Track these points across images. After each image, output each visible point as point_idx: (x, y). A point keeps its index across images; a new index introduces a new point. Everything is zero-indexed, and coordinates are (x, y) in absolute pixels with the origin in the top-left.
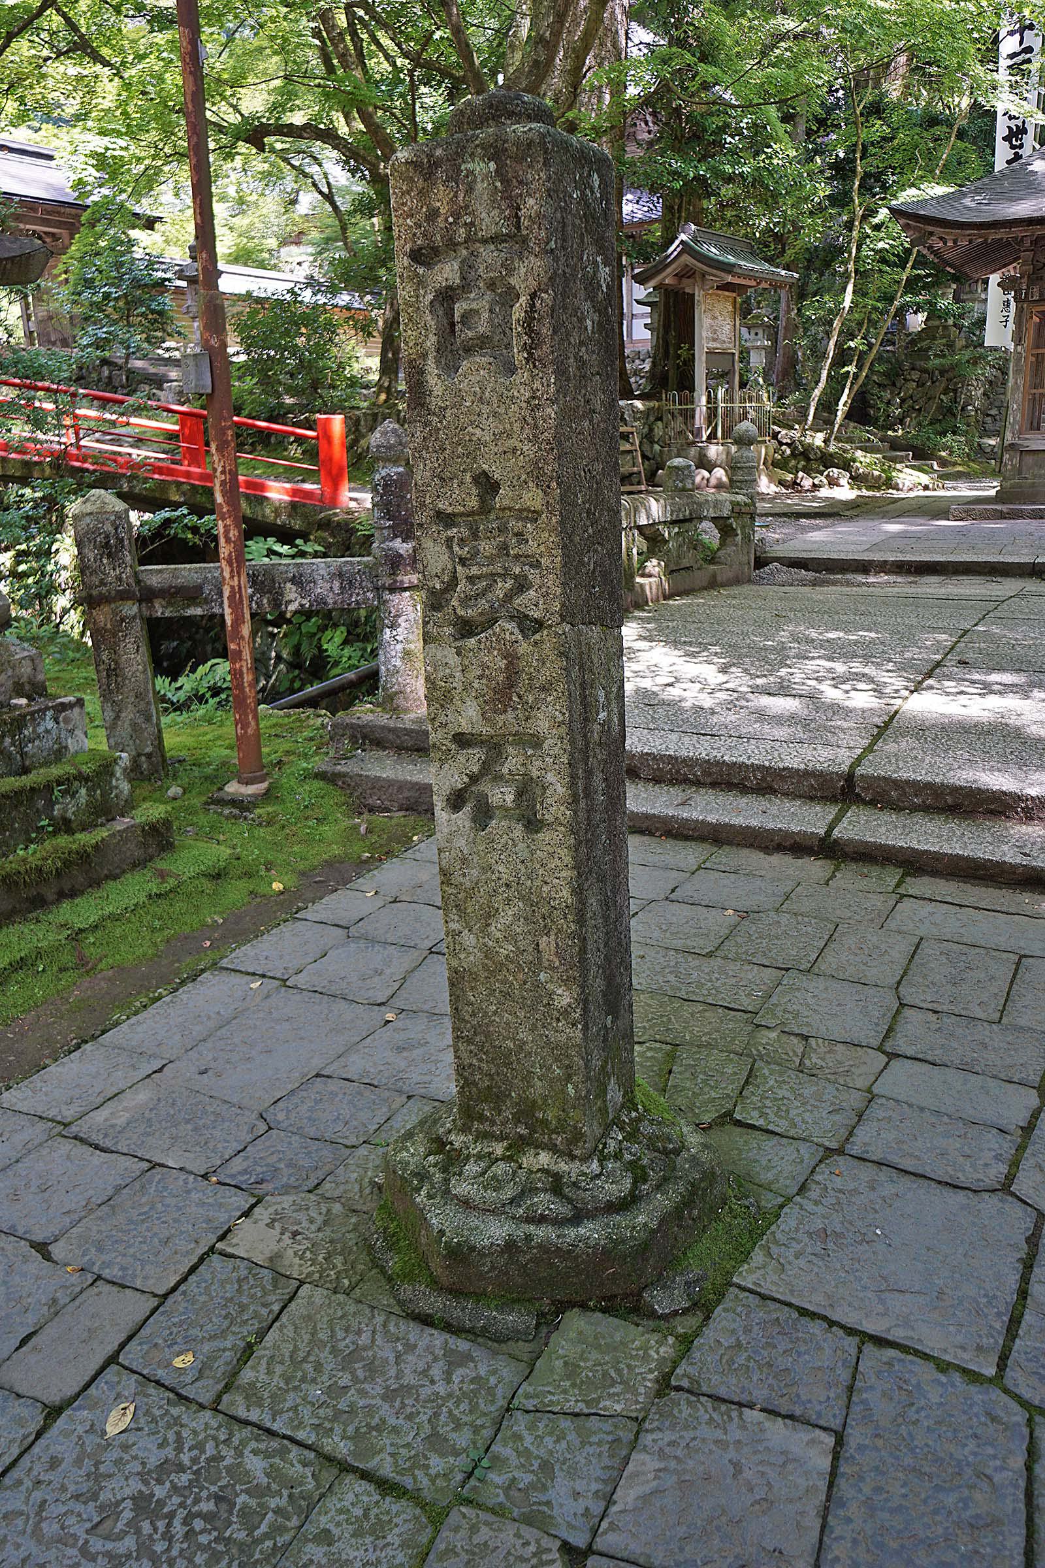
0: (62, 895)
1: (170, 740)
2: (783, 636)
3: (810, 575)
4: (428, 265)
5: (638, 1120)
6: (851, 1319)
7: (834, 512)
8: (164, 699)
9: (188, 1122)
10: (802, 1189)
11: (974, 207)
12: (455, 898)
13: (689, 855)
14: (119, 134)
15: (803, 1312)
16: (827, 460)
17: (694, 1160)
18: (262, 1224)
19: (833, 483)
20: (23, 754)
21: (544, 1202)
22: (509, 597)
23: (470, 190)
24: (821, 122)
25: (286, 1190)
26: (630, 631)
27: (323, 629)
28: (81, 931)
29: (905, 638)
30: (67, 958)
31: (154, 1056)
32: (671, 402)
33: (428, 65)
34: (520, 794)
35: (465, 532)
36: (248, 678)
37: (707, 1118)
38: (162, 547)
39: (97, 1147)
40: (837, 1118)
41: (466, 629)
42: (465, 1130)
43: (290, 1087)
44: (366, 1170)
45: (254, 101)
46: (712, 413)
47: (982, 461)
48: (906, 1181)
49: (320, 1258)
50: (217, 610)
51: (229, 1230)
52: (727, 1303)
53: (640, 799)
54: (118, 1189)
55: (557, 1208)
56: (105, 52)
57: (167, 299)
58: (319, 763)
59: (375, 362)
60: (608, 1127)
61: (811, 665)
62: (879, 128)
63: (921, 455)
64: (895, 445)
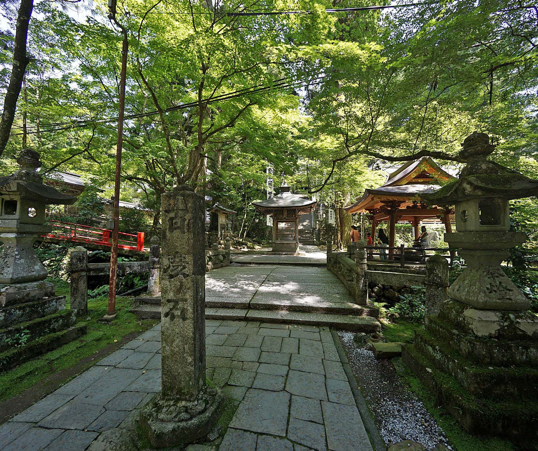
0: (48, 350)
1: (89, 305)
2: (236, 276)
3: (240, 265)
4: (168, 213)
5: (207, 388)
6: (254, 430)
7: (244, 253)
8: (89, 295)
9: (80, 413)
10: (244, 398)
11: (265, 204)
12: (165, 338)
13: (217, 323)
14: (98, 175)
15: (245, 431)
16: (243, 244)
17: (219, 396)
18: (100, 442)
19: (244, 248)
20: (44, 312)
21: (184, 415)
22: (181, 270)
23: (178, 201)
24: (240, 188)
25: (109, 429)
26: (206, 276)
27: (134, 277)
28: (53, 360)
29: (258, 276)
30: (46, 369)
31: (71, 395)
32: (214, 232)
33: (169, 172)
34: (182, 312)
35: (173, 257)
36: (114, 289)
37: (222, 385)
38: (95, 259)
39: (46, 428)
40: (250, 379)
41: (171, 277)
42: (163, 399)
43: (113, 397)
44: (134, 417)
45: (130, 172)
46: (221, 235)
47: (269, 245)
48: (265, 392)
49: (118, 448)
50: (108, 273)
51: (89, 446)
52: (227, 433)
53: (209, 312)
54: (52, 441)
55: (187, 416)
56: (97, 159)
57: (104, 206)
58: (130, 309)
59: (152, 222)
60: (199, 392)
61: (241, 282)
62: (249, 190)
63: (259, 243)
64: (254, 241)
